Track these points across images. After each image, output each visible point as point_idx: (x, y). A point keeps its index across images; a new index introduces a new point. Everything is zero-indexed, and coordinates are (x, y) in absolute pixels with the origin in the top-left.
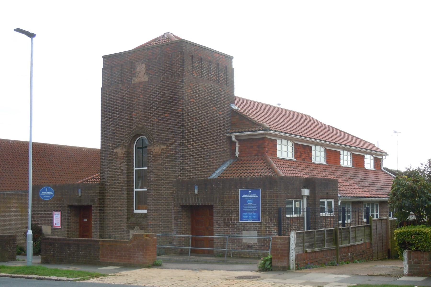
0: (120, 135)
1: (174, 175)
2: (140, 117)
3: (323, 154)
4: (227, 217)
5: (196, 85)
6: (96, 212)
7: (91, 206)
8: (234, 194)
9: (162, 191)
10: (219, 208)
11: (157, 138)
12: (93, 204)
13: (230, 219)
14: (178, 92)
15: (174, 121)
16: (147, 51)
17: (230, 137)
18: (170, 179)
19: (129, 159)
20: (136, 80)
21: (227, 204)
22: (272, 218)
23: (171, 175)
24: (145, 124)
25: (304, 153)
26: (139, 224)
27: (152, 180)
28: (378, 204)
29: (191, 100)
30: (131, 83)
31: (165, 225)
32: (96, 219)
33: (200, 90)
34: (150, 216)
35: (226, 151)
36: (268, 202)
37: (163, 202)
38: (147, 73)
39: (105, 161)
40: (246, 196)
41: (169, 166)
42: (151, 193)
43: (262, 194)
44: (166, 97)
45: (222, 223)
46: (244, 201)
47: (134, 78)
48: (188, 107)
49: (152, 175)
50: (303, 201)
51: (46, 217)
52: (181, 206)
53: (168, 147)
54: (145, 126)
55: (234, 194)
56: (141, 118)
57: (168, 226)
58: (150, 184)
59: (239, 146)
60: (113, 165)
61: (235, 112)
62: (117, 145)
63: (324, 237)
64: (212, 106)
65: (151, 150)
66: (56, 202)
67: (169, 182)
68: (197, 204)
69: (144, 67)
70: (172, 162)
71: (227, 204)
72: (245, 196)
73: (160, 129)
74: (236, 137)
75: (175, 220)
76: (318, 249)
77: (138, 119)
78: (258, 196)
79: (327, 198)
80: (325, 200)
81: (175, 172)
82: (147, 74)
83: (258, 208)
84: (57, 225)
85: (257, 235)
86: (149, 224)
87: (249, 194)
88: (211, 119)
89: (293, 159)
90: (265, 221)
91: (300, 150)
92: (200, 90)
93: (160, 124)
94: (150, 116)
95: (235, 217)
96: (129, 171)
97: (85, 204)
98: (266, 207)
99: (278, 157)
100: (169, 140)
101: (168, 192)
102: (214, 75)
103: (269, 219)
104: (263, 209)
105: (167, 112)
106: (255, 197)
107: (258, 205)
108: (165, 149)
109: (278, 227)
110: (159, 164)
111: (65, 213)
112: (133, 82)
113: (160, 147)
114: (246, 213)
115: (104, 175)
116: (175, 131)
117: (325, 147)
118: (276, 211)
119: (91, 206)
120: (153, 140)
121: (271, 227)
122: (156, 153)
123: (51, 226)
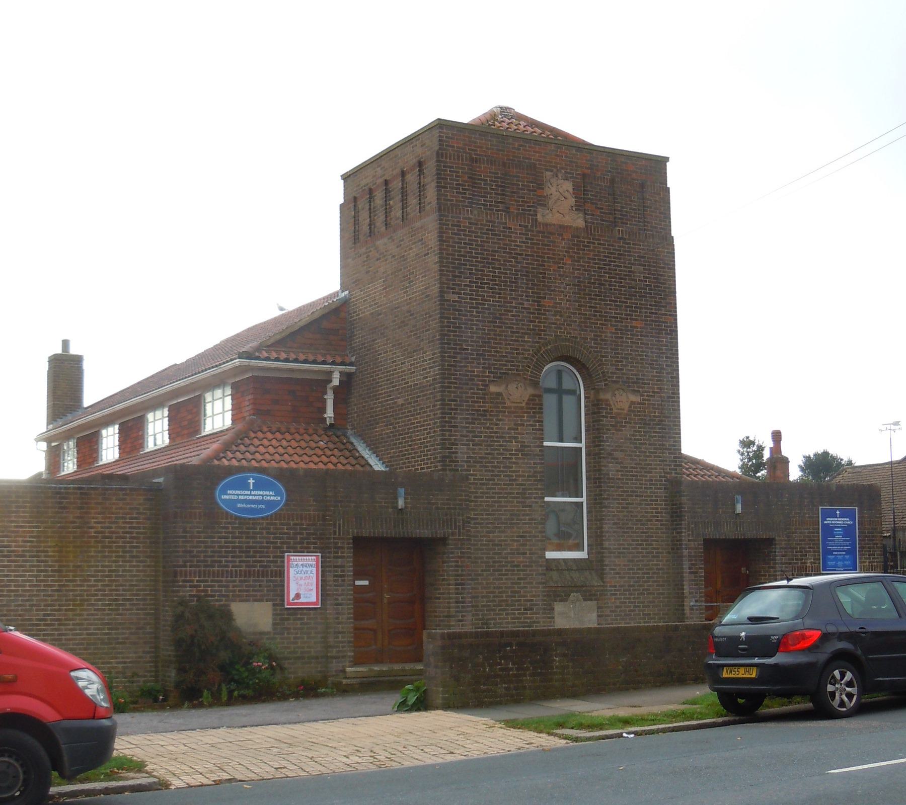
0: (507, 349)
1: (660, 469)
4: (797, 563)
8: (810, 517)
11: (615, 373)
12: (453, 534)
13: (803, 568)
14: (664, 276)
15: (656, 341)
16: (574, 152)
18: (650, 477)
21: (796, 536)
22: (876, 564)
24: (580, 334)
26: (583, 586)
31: (641, 588)
32: (462, 575)
36: (868, 533)
37: (635, 532)
39: (459, 414)
40: (238, 495)
42: (609, 507)
46: (829, 531)
49: (612, 463)
51: (247, 574)
54: (582, 338)
55: (810, 517)
56: (570, 317)
57: (649, 590)
58: (608, 487)
59: (325, 416)
60: (488, 428)
65: (607, 400)
66: (295, 524)
67: (648, 483)
68: (735, 536)
71: (796, 536)
72: (830, 521)
73: (622, 354)
75: (690, 573)
77: (561, 316)
78: (852, 523)
81: (663, 461)
84: (302, 600)
86: (606, 586)
87: (837, 517)
93: (622, 342)
100: (645, 384)
101: (647, 508)
105: (639, 316)
106: (846, 522)
108: (639, 404)
110: (626, 439)
113: (628, 397)
115: (457, 453)
116: (660, 365)
118: (150, 648)
120: (604, 376)
122: (619, 411)
123: (271, 603)
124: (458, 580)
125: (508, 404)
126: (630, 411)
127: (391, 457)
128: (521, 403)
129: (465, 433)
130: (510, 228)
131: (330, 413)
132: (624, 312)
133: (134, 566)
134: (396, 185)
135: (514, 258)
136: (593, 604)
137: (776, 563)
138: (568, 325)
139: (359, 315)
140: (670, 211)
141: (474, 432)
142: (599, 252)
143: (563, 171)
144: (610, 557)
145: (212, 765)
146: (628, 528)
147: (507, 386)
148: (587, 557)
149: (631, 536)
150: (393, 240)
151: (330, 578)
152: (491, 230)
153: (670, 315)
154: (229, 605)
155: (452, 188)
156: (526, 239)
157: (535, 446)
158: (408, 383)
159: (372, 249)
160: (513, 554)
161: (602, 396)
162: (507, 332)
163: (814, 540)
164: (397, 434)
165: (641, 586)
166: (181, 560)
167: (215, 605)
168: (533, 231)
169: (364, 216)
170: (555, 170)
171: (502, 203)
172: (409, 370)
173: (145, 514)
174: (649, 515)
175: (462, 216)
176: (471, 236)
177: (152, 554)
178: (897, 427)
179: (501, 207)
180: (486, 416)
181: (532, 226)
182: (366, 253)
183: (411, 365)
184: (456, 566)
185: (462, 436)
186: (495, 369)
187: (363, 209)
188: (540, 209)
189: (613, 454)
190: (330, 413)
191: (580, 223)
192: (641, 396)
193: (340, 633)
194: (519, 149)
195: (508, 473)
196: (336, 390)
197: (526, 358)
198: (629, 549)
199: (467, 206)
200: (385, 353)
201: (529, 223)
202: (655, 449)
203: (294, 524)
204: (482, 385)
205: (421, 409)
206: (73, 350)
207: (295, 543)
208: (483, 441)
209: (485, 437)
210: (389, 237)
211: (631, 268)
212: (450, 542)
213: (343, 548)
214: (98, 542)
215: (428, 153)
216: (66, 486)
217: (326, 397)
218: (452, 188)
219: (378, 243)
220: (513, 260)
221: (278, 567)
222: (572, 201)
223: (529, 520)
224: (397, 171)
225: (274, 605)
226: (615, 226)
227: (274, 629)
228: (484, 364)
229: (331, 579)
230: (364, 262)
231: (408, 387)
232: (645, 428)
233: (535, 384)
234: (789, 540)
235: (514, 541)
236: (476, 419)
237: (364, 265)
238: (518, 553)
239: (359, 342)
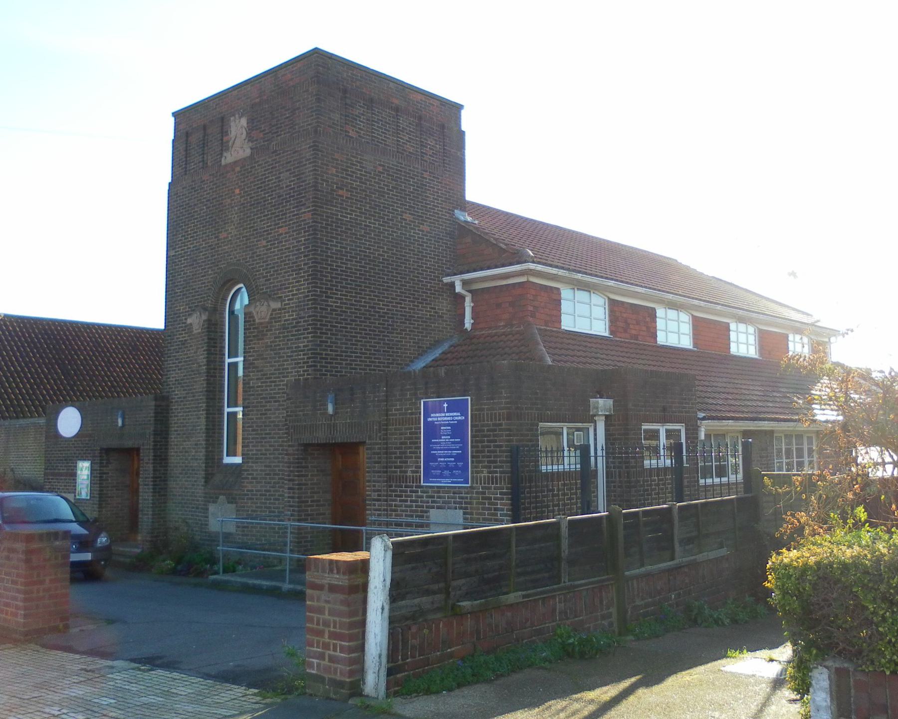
3: (686, 328)
5: (354, 159)
7: (138, 450)
10: (380, 449)
13: (403, 477)
17: (452, 285)
19: (213, 339)
20: (229, 158)
25: (635, 322)
28: (814, 436)
29: (340, 192)
30: (221, 164)
33: (365, 172)
34: (246, 470)
35: (442, 317)
36: (488, 431)
38: (249, 138)
43: (472, 411)
44: (283, 188)
45: (385, 488)
46: (432, 430)
47: (225, 154)
48: (330, 209)
50: (595, 430)
52: (300, 445)
53: (285, 305)
61: (463, 229)
63: (559, 546)
64: (402, 212)
69: (245, 125)
74: (465, 283)
76: (524, 596)
79: (664, 420)
80: (658, 427)
82: (249, 141)
83: (464, 449)
85: (461, 521)
88: (397, 240)
89: (607, 334)
90: (481, 484)
91: (625, 315)
92: (365, 172)
94: (253, 235)
95: (413, 472)
96: (212, 366)
97: (129, 444)
98: (482, 447)
99: (563, 328)
102: (407, 141)
103: (489, 477)
104: (477, 452)
106: (456, 418)
107: (464, 442)
108: (280, 309)
109: (512, 499)
112: (223, 162)
113: (269, 306)
114: (437, 461)
117: (690, 311)
119: (138, 450)
121: (496, 499)
126: (271, 319)
136: (233, 506)
146: (266, 434)
149: (269, 442)
165: (277, 491)
189: (254, 363)
190: (468, 323)
198: (266, 454)
214: (330, 346)
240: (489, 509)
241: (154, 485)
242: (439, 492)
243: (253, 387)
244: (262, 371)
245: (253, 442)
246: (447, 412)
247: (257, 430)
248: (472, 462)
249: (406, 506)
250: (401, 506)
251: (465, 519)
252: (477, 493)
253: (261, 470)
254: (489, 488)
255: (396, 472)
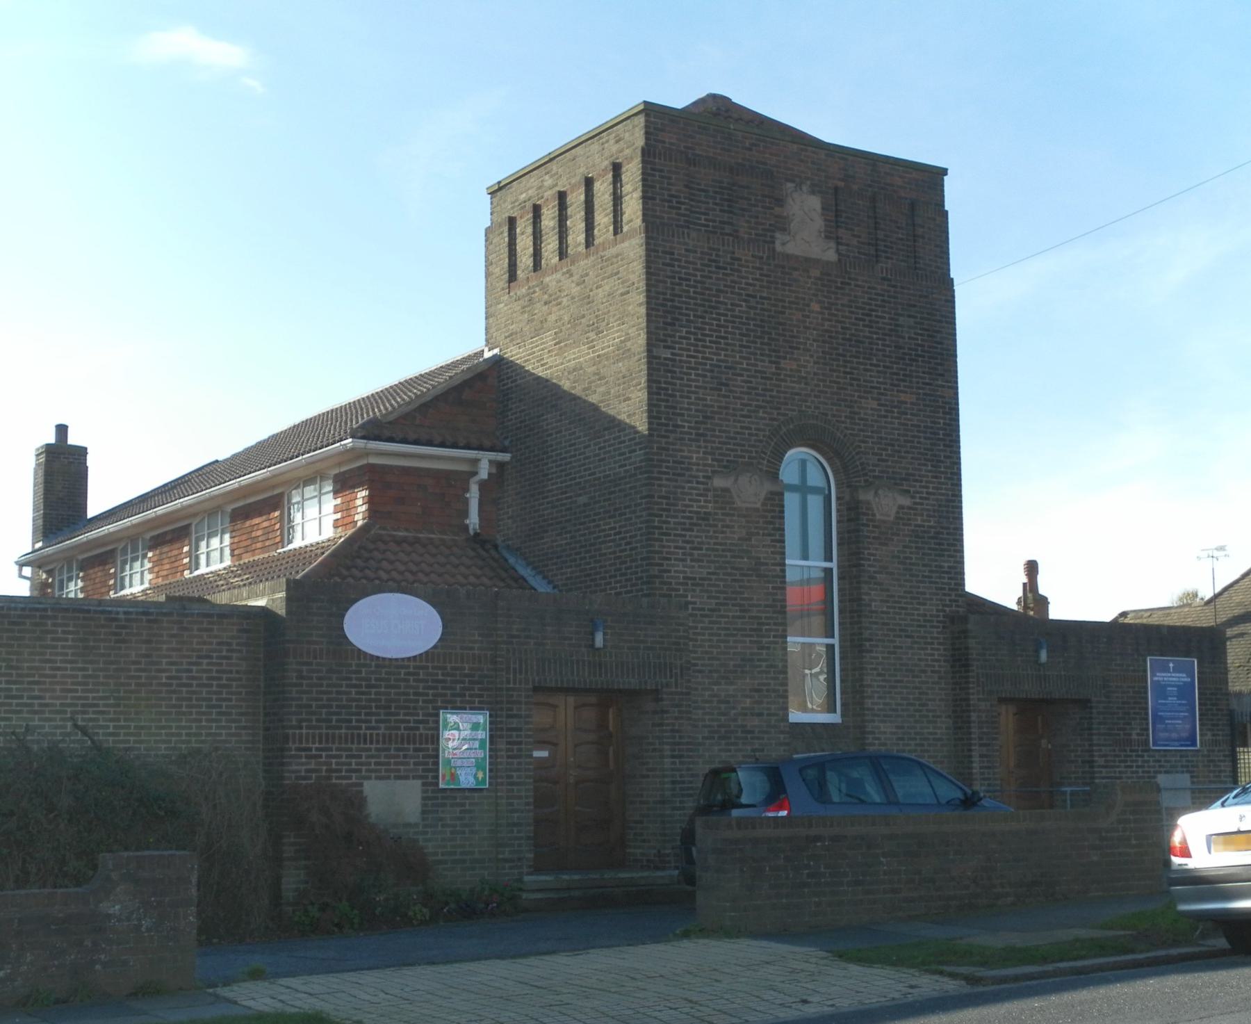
2: (812, 379)
6: (676, 718)
7: (656, 694)
9: (901, 648)
12: (667, 685)
18: (924, 610)
23: (928, 596)
27: (873, 609)
32: (679, 744)
41: (921, 568)
49: (876, 590)
59: (467, 522)
62: (725, 463)
65: (868, 503)
66: (453, 668)
70: (930, 555)
72: (1160, 677)
75: (981, 745)
77: (806, 384)
95: (1138, 734)
108: (909, 508)
111: (515, 720)
120: (863, 469)
124: (674, 751)
125: (739, 504)
126: (897, 518)
127: (567, 579)
128: (755, 503)
129: (680, 544)
130: (739, 259)
131: (473, 520)
132: (889, 381)
133: (223, 727)
134: (576, 199)
135: (745, 301)
137: (1092, 734)
138: (815, 396)
139: (516, 381)
140: (948, 244)
141: (693, 542)
142: (855, 297)
143: (809, 183)
144: (873, 721)
145: (766, 997)
147: (736, 480)
148: (418, 783)
150: (571, 275)
151: (502, 746)
152: (715, 261)
153: (949, 387)
154: (361, 785)
155: (663, 200)
156: (761, 275)
157: (773, 565)
158: (594, 473)
159: (537, 289)
160: (745, 715)
161: (862, 496)
162: (736, 404)
163: (1140, 703)
164: (578, 545)
166: (294, 718)
167: (341, 784)
168: (769, 265)
169: (525, 243)
170: (797, 180)
171: (729, 223)
172: (595, 456)
173: (240, 651)
174: (923, 663)
175: (676, 239)
176: (688, 268)
177: (250, 710)
178: (1222, 553)
179: (728, 229)
180: (708, 520)
181: (768, 258)
182: (528, 294)
183: (600, 449)
184: (672, 731)
185: (676, 547)
186: (720, 454)
187: (523, 234)
188: (778, 235)
189: (876, 578)
190: (473, 520)
191: (831, 256)
192: (913, 497)
193: (515, 825)
194: (750, 150)
195: (738, 601)
196: (483, 485)
197: (761, 441)
199: (682, 226)
200: (557, 433)
201: (764, 253)
202: (930, 571)
203: (452, 668)
204: (704, 477)
205: (616, 510)
206: (72, 440)
207: (453, 695)
208: (705, 555)
209: (707, 549)
210: (565, 270)
211: (897, 320)
212: (665, 696)
213: (520, 703)
215: (627, 152)
216: (126, 609)
217: (468, 495)
218: (663, 200)
219: (547, 279)
220: (744, 304)
221: (429, 729)
222: (819, 223)
223: (767, 667)
224: (578, 179)
225: (424, 784)
226: (877, 261)
227: (423, 819)
228: (706, 447)
229: (503, 747)
230: (524, 307)
231: (595, 479)
232: (917, 542)
233: (774, 476)
234: (1109, 702)
235: (747, 696)
236: (695, 525)
237: (525, 312)
238: (752, 715)
239: (516, 418)
240: (1214, 771)
241: (970, 756)
242: (1165, 756)
243: (876, 612)
244: (888, 590)
245: (878, 692)
246: (1174, 672)
247: (884, 675)
248: (1148, 724)
249: (1132, 772)
250: (1126, 772)
251: (1193, 783)
252: (1203, 756)
253: (892, 733)
254: (1213, 751)
255: (1119, 735)
